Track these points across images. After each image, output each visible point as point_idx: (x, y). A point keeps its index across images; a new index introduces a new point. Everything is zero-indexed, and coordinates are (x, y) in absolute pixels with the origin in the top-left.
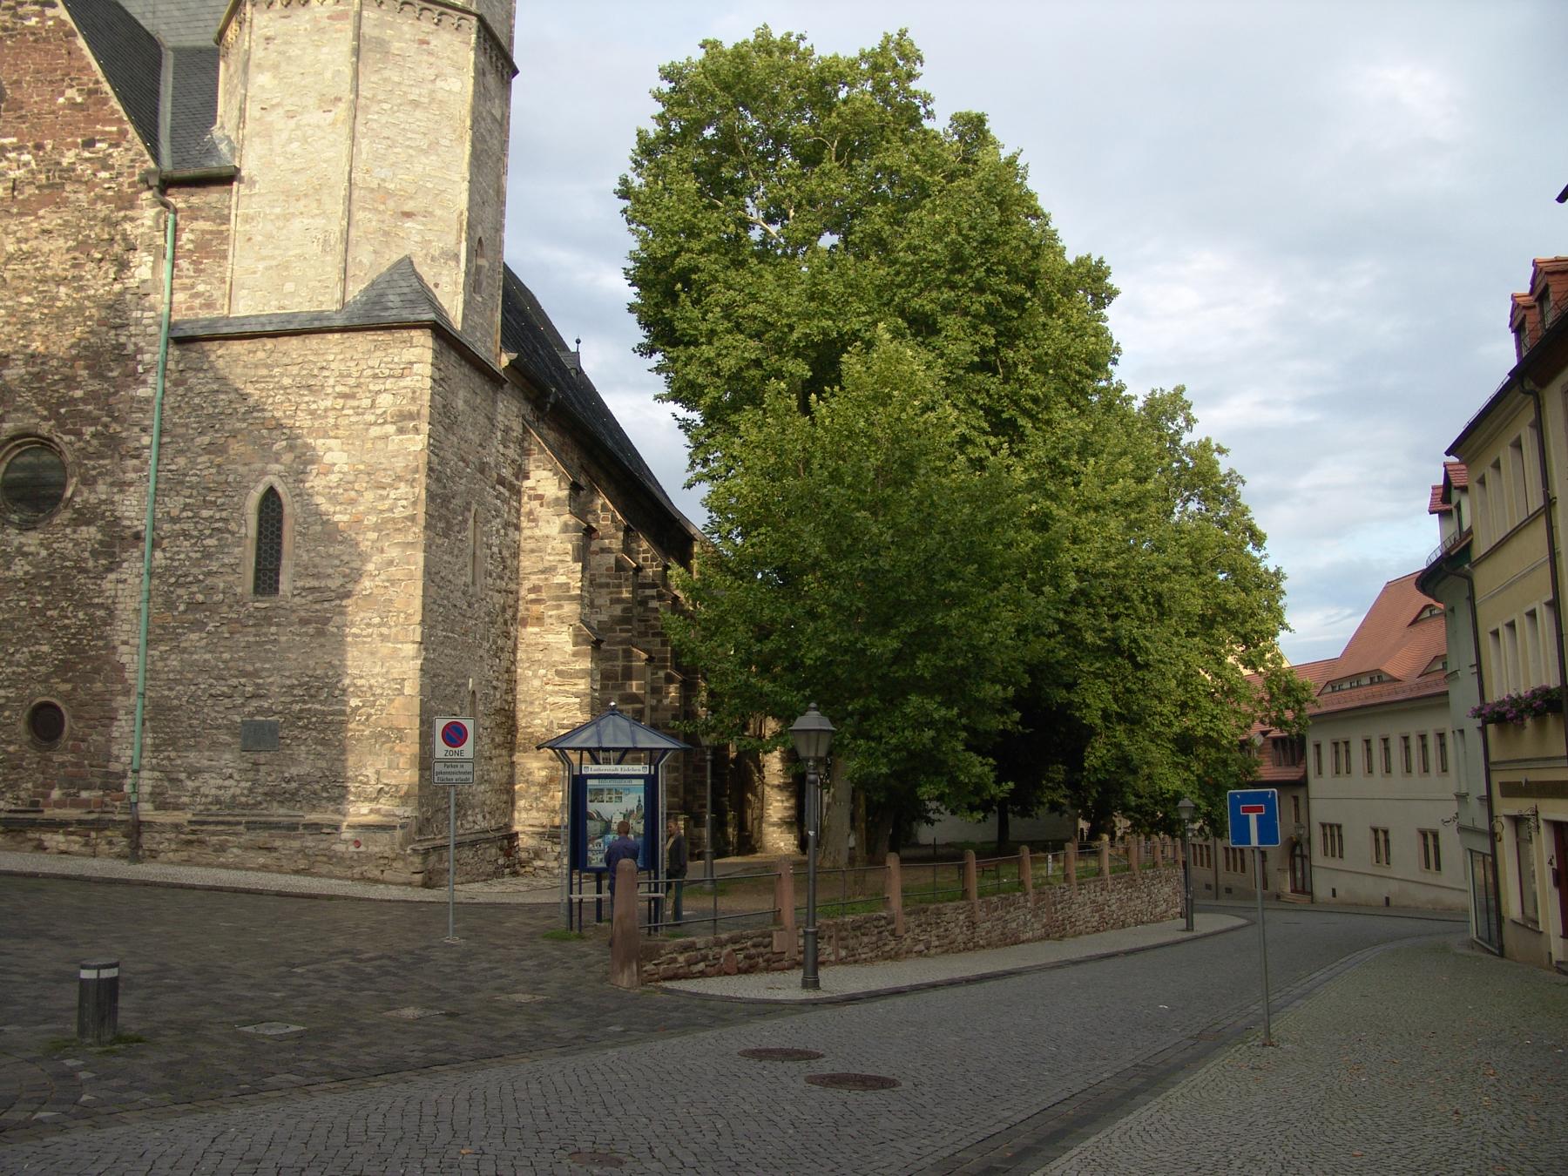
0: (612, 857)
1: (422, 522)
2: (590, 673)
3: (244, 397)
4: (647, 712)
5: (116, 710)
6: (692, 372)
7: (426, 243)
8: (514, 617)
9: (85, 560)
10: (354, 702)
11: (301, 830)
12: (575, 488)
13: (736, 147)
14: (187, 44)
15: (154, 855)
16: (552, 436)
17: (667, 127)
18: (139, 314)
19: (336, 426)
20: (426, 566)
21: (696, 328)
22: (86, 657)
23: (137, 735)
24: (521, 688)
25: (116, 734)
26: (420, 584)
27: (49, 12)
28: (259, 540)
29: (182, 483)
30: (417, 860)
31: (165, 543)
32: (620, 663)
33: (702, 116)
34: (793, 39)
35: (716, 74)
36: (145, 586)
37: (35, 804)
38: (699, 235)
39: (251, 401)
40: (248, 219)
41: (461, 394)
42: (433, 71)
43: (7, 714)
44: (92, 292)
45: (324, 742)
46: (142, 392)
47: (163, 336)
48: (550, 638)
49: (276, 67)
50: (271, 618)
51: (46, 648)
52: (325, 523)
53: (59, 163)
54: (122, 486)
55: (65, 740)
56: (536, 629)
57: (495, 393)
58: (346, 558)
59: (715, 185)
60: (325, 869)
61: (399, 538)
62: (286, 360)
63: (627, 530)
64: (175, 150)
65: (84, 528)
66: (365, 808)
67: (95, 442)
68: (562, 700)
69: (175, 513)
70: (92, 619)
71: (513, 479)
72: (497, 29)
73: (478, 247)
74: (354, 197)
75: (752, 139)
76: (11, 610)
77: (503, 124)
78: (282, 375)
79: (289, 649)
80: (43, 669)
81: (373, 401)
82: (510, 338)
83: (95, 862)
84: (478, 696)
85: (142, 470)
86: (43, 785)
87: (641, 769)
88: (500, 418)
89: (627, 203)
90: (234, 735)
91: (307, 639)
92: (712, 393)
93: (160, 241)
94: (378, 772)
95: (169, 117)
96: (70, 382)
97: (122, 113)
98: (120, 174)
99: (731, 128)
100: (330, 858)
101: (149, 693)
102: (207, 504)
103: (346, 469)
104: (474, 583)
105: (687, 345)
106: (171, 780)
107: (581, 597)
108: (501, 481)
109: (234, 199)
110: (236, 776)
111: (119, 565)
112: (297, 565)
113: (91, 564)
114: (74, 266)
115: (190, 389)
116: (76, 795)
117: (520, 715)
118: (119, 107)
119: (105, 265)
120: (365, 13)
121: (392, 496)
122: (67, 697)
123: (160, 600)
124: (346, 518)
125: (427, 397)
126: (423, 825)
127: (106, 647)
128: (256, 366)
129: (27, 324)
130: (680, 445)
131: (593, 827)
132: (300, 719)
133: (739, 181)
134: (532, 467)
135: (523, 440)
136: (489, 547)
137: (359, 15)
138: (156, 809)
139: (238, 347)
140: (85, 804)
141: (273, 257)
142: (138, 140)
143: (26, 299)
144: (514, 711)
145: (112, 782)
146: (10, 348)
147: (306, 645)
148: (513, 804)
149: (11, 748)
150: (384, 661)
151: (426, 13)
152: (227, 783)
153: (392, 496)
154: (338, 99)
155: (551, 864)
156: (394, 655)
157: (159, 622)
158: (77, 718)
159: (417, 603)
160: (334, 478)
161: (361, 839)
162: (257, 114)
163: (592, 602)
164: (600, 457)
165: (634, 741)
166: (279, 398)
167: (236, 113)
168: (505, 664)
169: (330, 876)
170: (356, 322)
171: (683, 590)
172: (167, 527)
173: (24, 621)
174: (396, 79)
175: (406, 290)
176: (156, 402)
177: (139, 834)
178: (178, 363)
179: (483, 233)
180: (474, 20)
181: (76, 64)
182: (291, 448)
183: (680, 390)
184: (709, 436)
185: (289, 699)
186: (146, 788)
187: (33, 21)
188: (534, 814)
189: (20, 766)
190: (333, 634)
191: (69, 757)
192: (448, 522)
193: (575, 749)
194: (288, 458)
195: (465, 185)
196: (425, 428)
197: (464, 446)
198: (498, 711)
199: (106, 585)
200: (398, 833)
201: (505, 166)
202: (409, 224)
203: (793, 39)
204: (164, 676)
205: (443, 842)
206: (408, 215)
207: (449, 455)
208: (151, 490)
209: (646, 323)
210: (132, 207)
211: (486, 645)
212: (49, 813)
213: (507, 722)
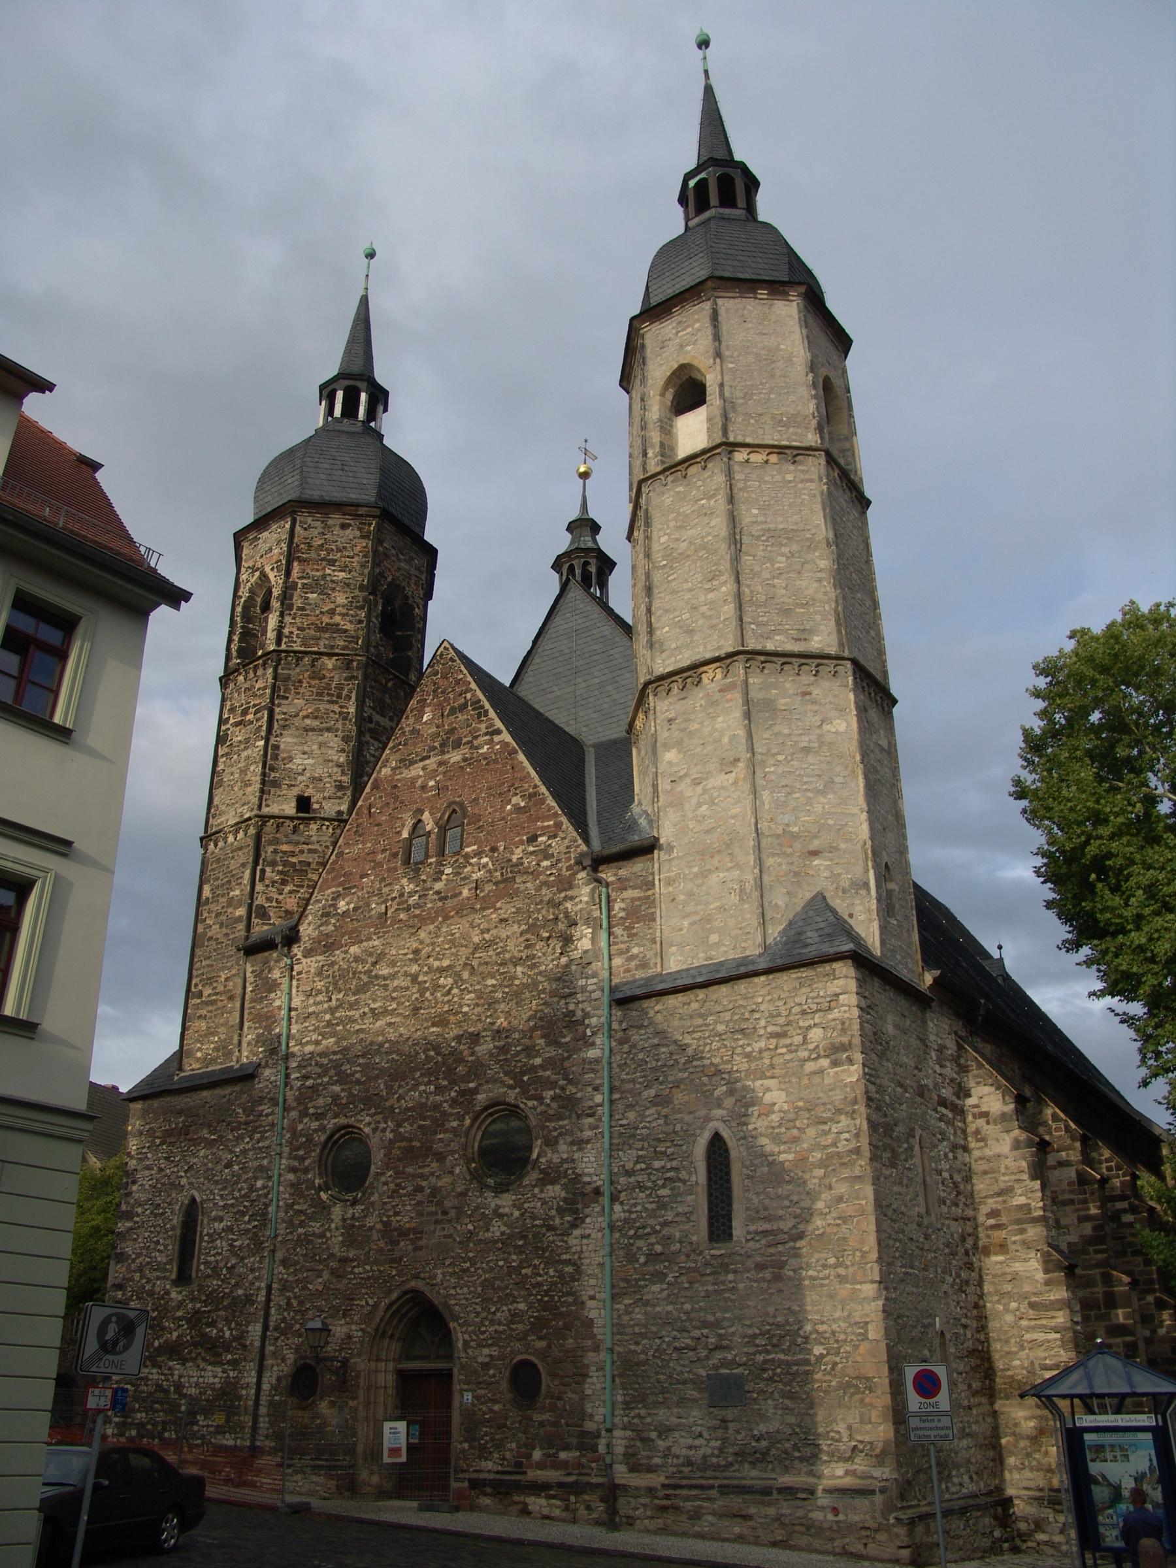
0: (1131, 1532)
1: (867, 1154)
3: (683, 1048)
4: (1141, 1346)
5: (587, 1367)
6: (1123, 963)
7: (835, 877)
8: (975, 1246)
10: (818, 1350)
11: (775, 1495)
12: (1020, 1100)
13: (1127, 725)
14: (604, 739)
15: (630, 1522)
16: (988, 1049)
19: (772, 1066)
21: (1120, 916)
22: (557, 1315)
23: (608, 1391)
24: (993, 1324)
25: (589, 1392)
26: (872, 1219)
27: (497, 738)
28: (709, 1186)
29: (633, 1136)
30: (902, 1531)
32: (1099, 1290)
34: (1162, 608)
35: (1091, 659)
36: (607, 1241)
37: (519, 1464)
38: (1106, 821)
39: (690, 1051)
40: (670, 882)
41: (890, 1018)
42: (818, 718)
43: (491, 1372)
44: (543, 968)
45: (791, 1395)
46: (592, 1053)
47: (606, 1000)
48: (1018, 1266)
50: (727, 1265)
51: (522, 1306)
52: (771, 1164)
53: (510, 860)
54: (580, 1144)
56: (1001, 1258)
58: (795, 1198)
59: (1114, 766)
60: (804, 1541)
61: (846, 1173)
63: (1084, 1140)
64: (602, 831)
65: (549, 1187)
67: (554, 1105)
68: (1040, 1336)
69: (629, 1166)
70: (561, 1275)
71: (954, 1098)
73: (884, 873)
74: (763, 845)
75: (1141, 715)
76: (491, 1269)
77: (891, 752)
78: (716, 1022)
80: (520, 1326)
81: (805, 1037)
82: (930, 957)
83: (575, 1529)
84: (948, 1336)
85: (597, 1127)
86: (526, 1445)
87: (1145, 1420)
88: (932, 1038)
89: (1024, 803)
90: (701, 1390)
91: (765, 1285)
92: (1150, 981)
93: (596, 914)
94: (849, 1428)
95: (595, 803)
96: (530, 1051)
97: (557, 808)
98: (559, 861)
99: (1117, 708)
101: (617, 1349)
102: (658, 1155)
103: (786, 1107)
105: (1114, 935)
106: (643, 1440)
108: (943, 1102)
109: (656, 866)
111: (583, 1221)
112: (748, 1209)
113: (557, 1221)
114: (527, 947)
115: (634, 1046)
116: (555, 1455)
117: (996, 1356)
118: (554, 804)
119: (552, 942)
120: (751, 680)
122: (543, 1354)
123: (621, 1253)
124: (791, 1157)
125: (856, 1026)
126: (905, 1489)
128: (691, 1017)
129: (492, 1004)
130: (1126, 1041)
131: (1100, 1493)
133: (1136, 758)
134: (972, 1084)
135: (959, 1057)
136: (939, 1173)
137: (746, 682)
138: (631, 1470)
139: (673, 1001)
140: (563, 1465)
141: (696, 913)
142: (571, 828)
143: (491, 982)
144: (988, 1352)
145: (587, 1443)
146: (480, 1026)
149: (497, 1407)
150: (844, 1304)
151: (805, 668)
152: (698, 1442)
154: (737, 760)
155: (1058, 1538)
156: (854, 1296)
158: (553, 1375)
159: (872, 1239)
160: (775, 1117)
161: (839, 1505)
163: (1057, 1221)
165: (1131, 1385)
167: (650, 789)
168: (972, 1298)
169: (810, 1550)
170: (779, 962)
171: (1159, 1201)
172: (622, 1180)
173: (503, 1280)
174: (786, 731)
175: (822, 925)
177: (615, 1499)
178: (621, 1022)
180: (849, 664)
181: (518, 775)
182: (731, 1092)
183: (1115, 983)
184: (1156, 1027)
185: (752, 1350)
186: (619, 1449)
188: (1028, 1474)
189: (505, 1426)
190: (790, 1279)
191: (547, 1416)
192: (893, 1151)
193: (1063, 1397)
194: (729, 1102)
195: (864, 816)
196: (859, 1057)
197: (900, 1071)
198: (972, 1352)
199: (572, 1241)
200: (878, 1499)
201: (899, 791)
203: (1162, 608)
204: (629, 1330)
205: (928, 1509)
206: (815, 853)
207: (886, 1082)
208: (607, 1146)
209: (1066, 917)
210: (571, 887)
211: (949, 1279)
212: (533, 1474)
213: (982, 1363)
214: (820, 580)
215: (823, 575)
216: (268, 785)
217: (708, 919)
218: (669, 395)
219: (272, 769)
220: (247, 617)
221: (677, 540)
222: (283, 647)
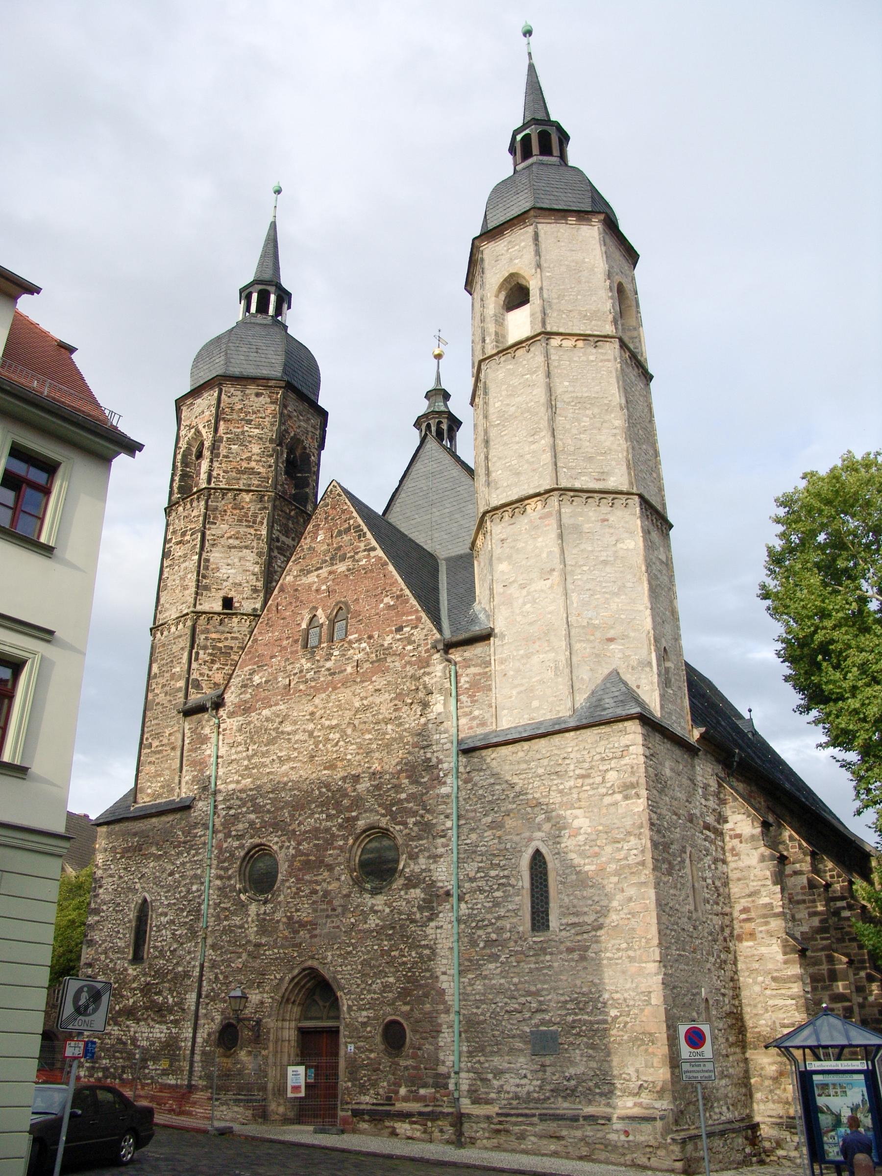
0: (849, 1148)
2: (801, 978)
3: (512, 786)
4: (856, 1009)
5: (440, 1025)
6: (842, 722)
8: (731, 934)
9: (414, 914)
10: (613, 1012)
11: (581, 1122)
12: (765, 825)
13: (845, 544)
14: (453, 554)
15: (473, 1141)
16: (741, 786)
17: (788, 541)
18: (438, 736)
19: (579, 800)
20: (657, 900)
21: (840, 687)
22: (418, 986)
23: (456, 1043)
25: (441, 1044)
28: (532, 890)
29: (475, 852)
30: (676, 1148)
31: (467, 897)
33: (815, 526)
34: (872, 456)
35: (818, 495)
36: (455, 931)
37: (389, 1098)
38: (830, 616)
39: (517, 788)
41: (668, 764)
42: (614, 538)
43: (369, 1029)
44: (407, 726)
45: (593, 1047)
46: (444, 790)
47: (454, 750)
48: (763, 950)
49: (509, 557)
50: (545, 949)
51: (392, 980)
53: (383, 645)
54: (435, 858)
55: (408, 1050)
56: (751, 943)
57: (694, 757)
58: (596, 898)
59: (835, 575)
60: (603, 1156)
61: (634, 880)
62: (539, 756)
63: (813, 855)
64: (452, 624)
65: (412, 890)
66: (629, 1102)
67: (416, 829)
68: (780, 1002)
69: (472, 874)
70: (421, 956)
71: (716, 824)
72: (654, 501)
73: (663, 654)
74: (572, 634)
75: (855, 536)
76: (369, 952)
77: (668, 564)
78: (537, 767)
79: (561, 972)
80: (390, 995)
81: (604, 778)
82: (698, 717)
83: (431, 1147)
84: (711, 1002)
85: (448, 845)
86: (394, 1084)
87: (859, 1065)
88: (699, 778)
89: (768, 602)
90: (525, 1043)
91: (573, 964)
92: (862, 736)
93: (447, 685)
94: (637, 1071)
95: (446, 602)
96: (397, 788)
97: (418, 606)
98: (419, 645)
99: (838, 531)
100: (606, 1146)
101: (463, 1011)
102: (493, 866)
103: (589, 830)
104: (696, 909)
105: (836, 701)
106: (482, 1080)
107: (783, 914)
108: (707, 827)
109: (492, 649)
110: (529, 1076)
112: (561, 907)
113: (418, 916)
114: (395, 710)
115: (475, 785)
116: (416, 1092)
117: (747, 1017)
119: (414, 706)
120: (563, 510)
121: (626, 847)
122: (407, 1016)
123: (466, 939)
124: (593, 868)
125: (642, 769)
126: (679, 1117)
127: (431, 977)
128: (518, 763)
130: (845, 781)
131: (825, 1120)
132: (573, 1028)
135: (719, 792)
136: (705, 879)
138: (473, 1103)
139: (504, 751)
140: (422, 1099)
141: (522, 685)
142: (428, 621)
143: (368, 736)
144: (741, 1014)
145: (440, 1082)
146: (360, 770)
147: (573, 968)
148: (751, 1096)
152: (523, 1081)
153: (626, 847)
154: (554, 570)
156: (641, 972)
157: (467, 956)
158: (415, 1031)
160: (581, 838)
161: (629, 1129)
162: (501, 590)
163: (793, 916)
164: (782, 798)
165: (848, 1038)
166: (536, 784)
167: (488, 592)
168: (729, 974)
169: (607, 1162)
170: (585, 722)
171: (869, 901)
172: (467, 885)
174: (590, 549)
175: (617, 694)
176: (454, 796)
177: (462, 1124)
178: (466, 767)
179: (667, 647)
180: (636, 498)
181: (389, 581)
182: (548, 819)
183: (837, 737)
184: (867, 770)
185: (564, 1012)
186: (464, 1087)
187: (363, 562)
188: (771, 1105)
189: (378, 1069)
190: (593, 959)
191: (410, 1062)
192: (670, 863)
193: (798, 1047)
194: (547, 826)
195: (648, 612)
196: (644, 793)
197: (675, 803)
198: (729, 1014)
199: (429, 931)
200: (659, 1124)
201: (674, 593)
202: (612, 646)
203: (872, 456)
204: (472, 998)
205: (696, 1132)
206: (611, 640)
207: (664, 812)
208: (455, 859)
210: (428, 666)
211: (712, 960)
212: (400, 1106)
213: (736, 1022)
214: (615, 435)
215: (617, 431)
216: (200, 589)
217: (531, 690)
218: (502, 296)
219: (204, 577)
220: (185, 463)
221: (508, 405)
222: (213, 485)
